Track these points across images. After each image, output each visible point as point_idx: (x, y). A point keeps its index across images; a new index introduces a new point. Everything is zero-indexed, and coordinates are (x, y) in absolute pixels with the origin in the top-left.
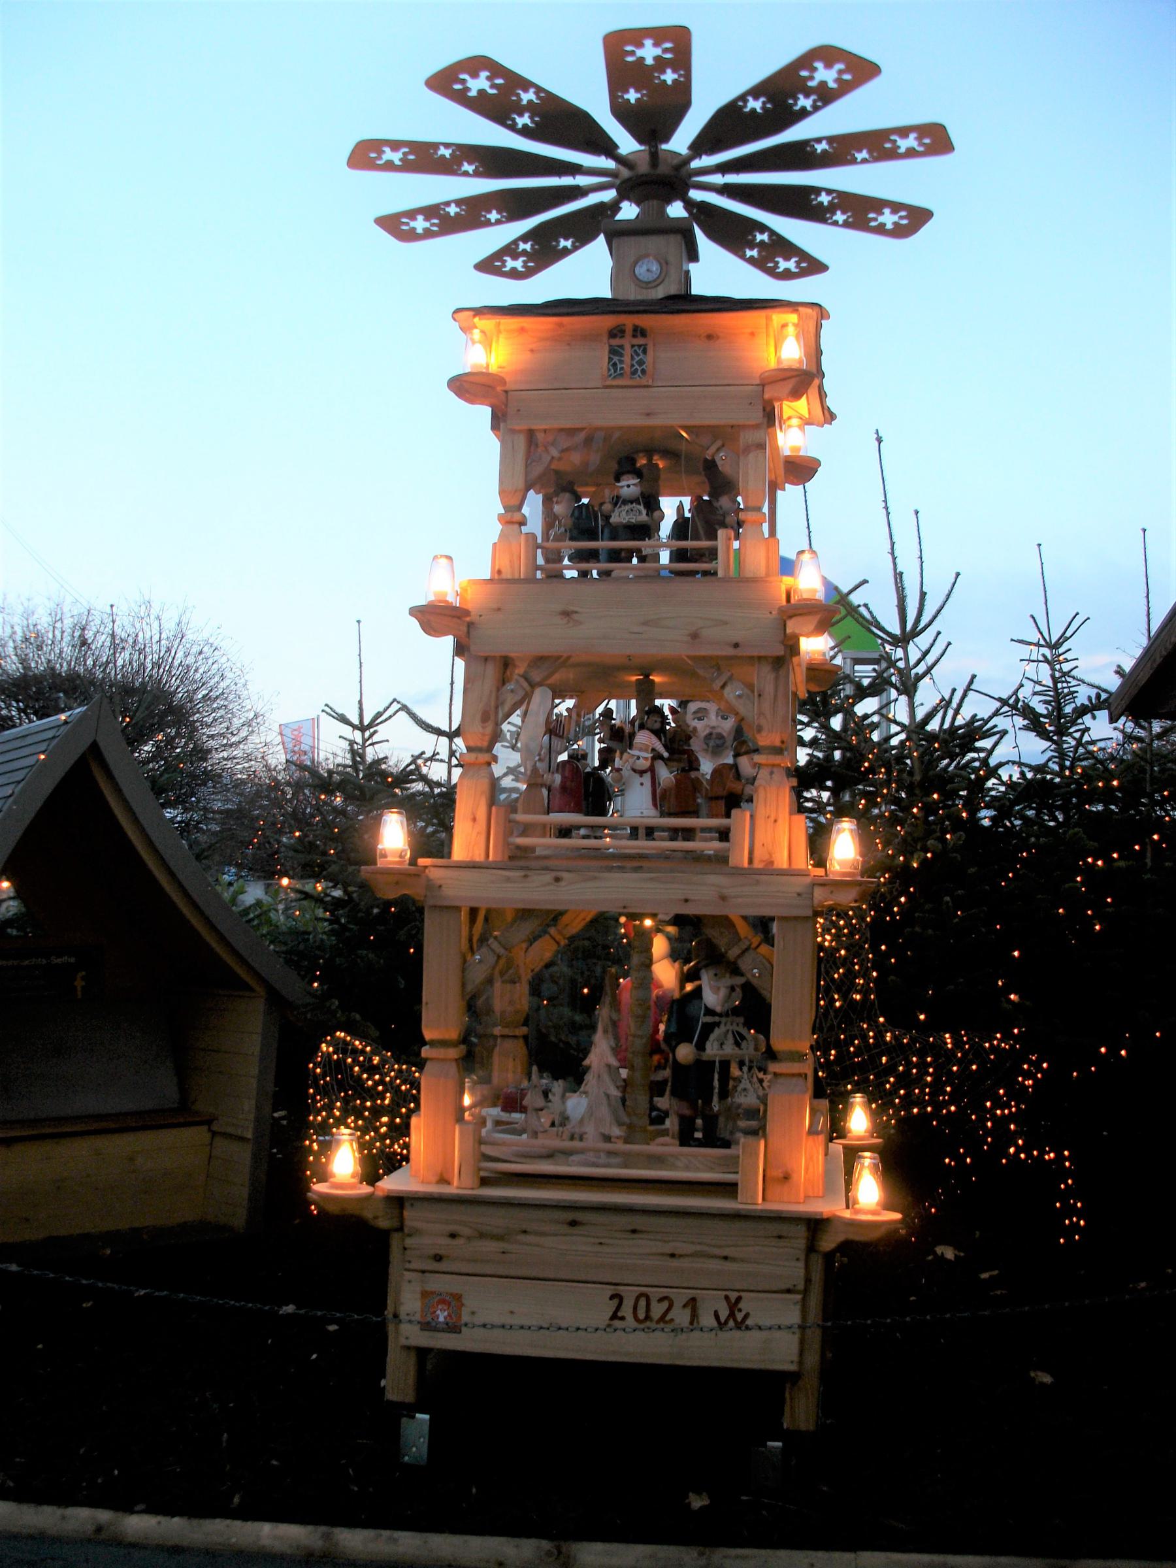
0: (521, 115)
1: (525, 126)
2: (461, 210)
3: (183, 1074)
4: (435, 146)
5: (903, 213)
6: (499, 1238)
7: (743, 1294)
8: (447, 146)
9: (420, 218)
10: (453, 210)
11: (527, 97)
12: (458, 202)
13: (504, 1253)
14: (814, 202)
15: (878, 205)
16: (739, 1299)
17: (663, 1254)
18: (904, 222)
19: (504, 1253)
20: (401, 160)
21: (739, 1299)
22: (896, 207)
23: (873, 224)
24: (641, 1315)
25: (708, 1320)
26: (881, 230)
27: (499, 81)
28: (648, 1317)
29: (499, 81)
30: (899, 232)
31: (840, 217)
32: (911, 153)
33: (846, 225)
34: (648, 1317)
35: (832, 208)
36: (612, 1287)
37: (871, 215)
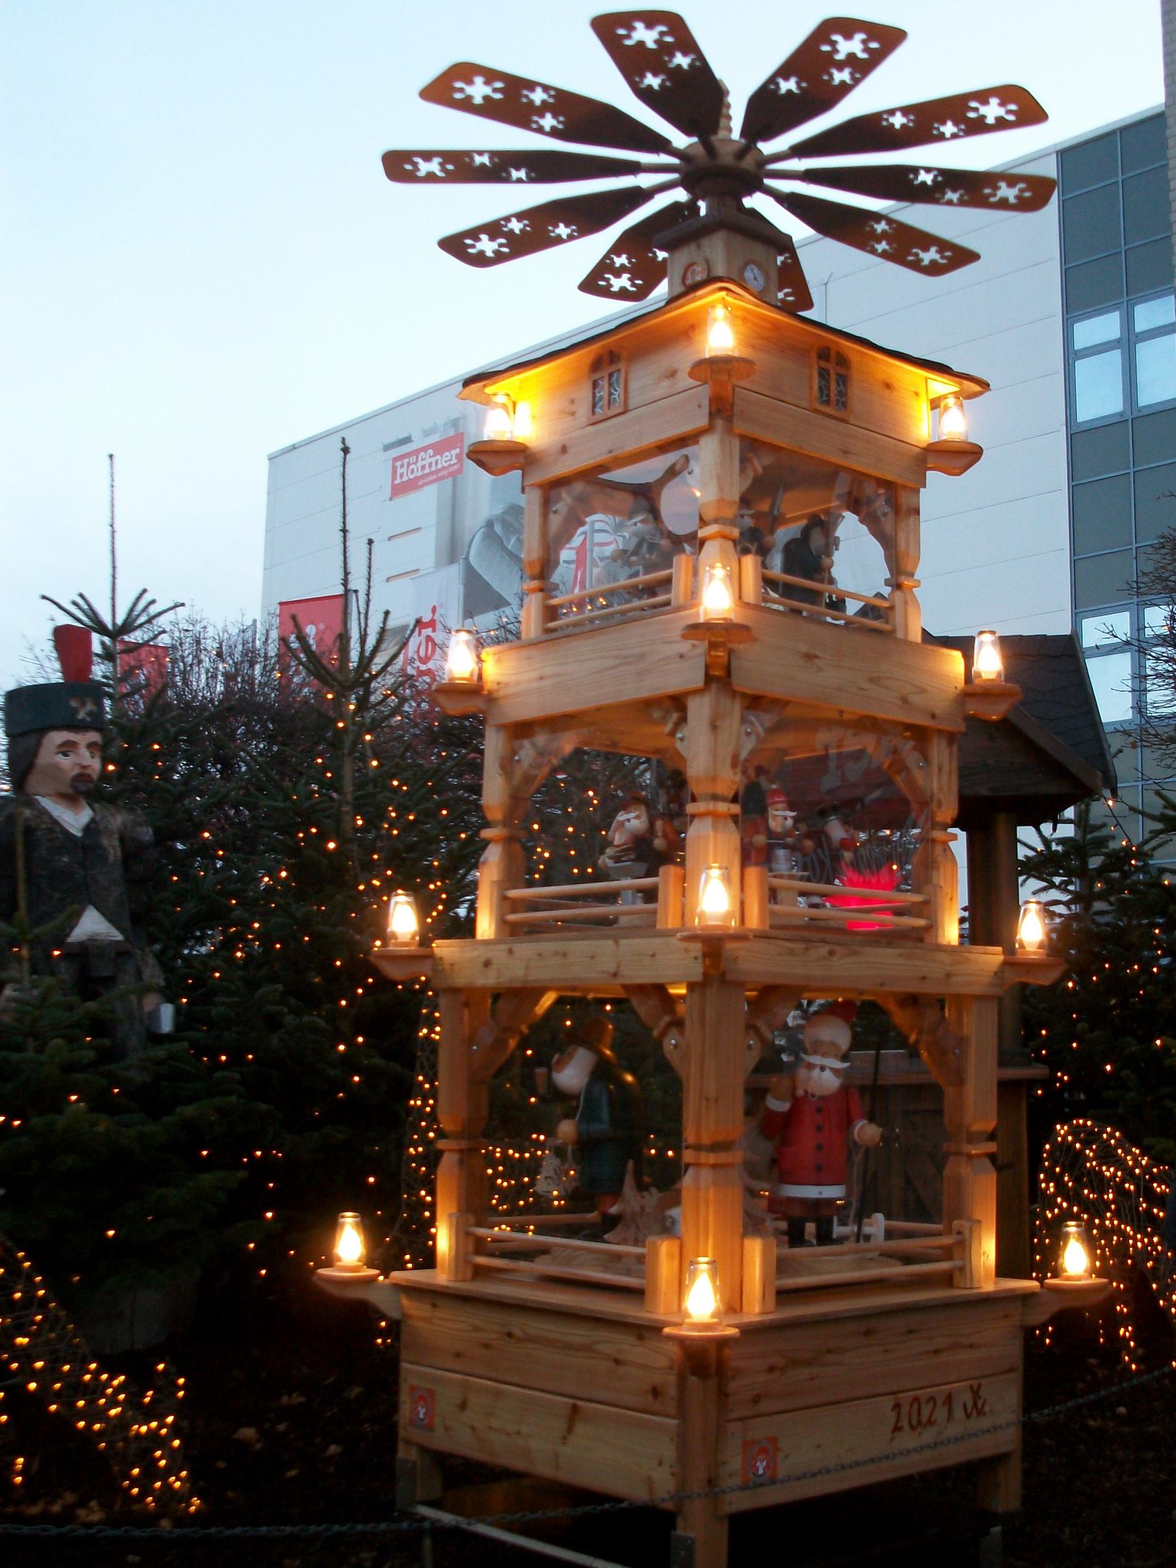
0: (884, 231)
1: (878, 222)
2: (938, 129)
3: (685, 870)
4: (962, 203)
5: (458, 96)
6: (809, 1363)
7: (983, 1381)
8: (950, 203)
9: (990, 120)
10: (949, 128)
11: (882, 246)
12: (941, 137)
13: (812, 1379)
14: (787, 255)
15: (488, 109)
16: (979, 1386)
17: (927, 1352)
18: (458, 85)
19: (812, 1379)
20: (999, 188)
21: (979, 1386)
22: (466, 105)
23: (499, 85)
24: (914, 1422)
25: (959, 1413)
26: (491, 75)
27: (948, 254)
28: (919, 1422)
29: (948, 254)
30: (465, 71)
31: (538, 96)
32: (431, 178)
33: (531, 85)
34: (919, 1422)
35: (545, 108)
36: (892, 1397)
37: (498, 96)
